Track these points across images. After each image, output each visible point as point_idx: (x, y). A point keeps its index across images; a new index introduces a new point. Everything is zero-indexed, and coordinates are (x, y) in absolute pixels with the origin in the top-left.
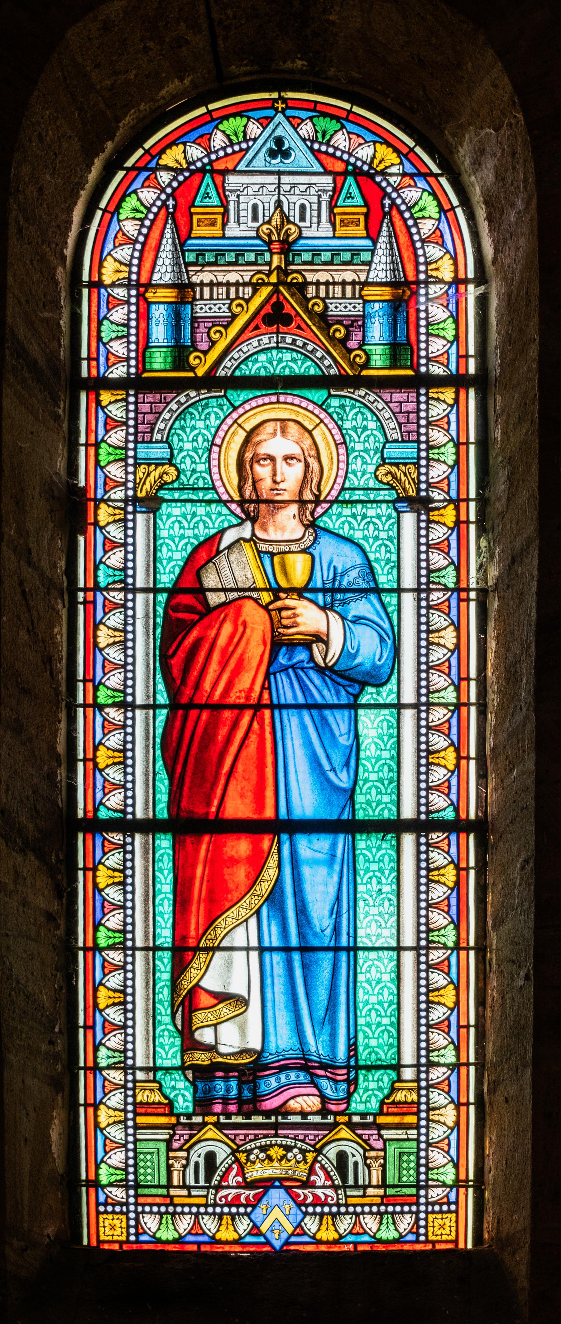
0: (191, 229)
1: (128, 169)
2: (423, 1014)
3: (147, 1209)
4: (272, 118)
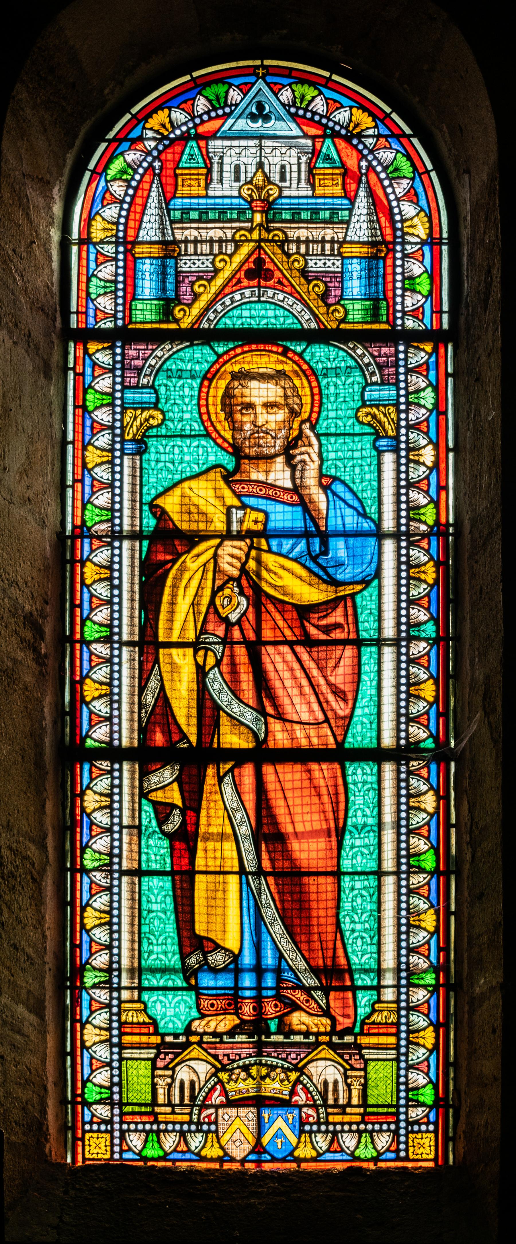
0: (176, 189)
1: (109, 141)
2: (404, 937)
3: (133, 1127)
4: (253, 84)
